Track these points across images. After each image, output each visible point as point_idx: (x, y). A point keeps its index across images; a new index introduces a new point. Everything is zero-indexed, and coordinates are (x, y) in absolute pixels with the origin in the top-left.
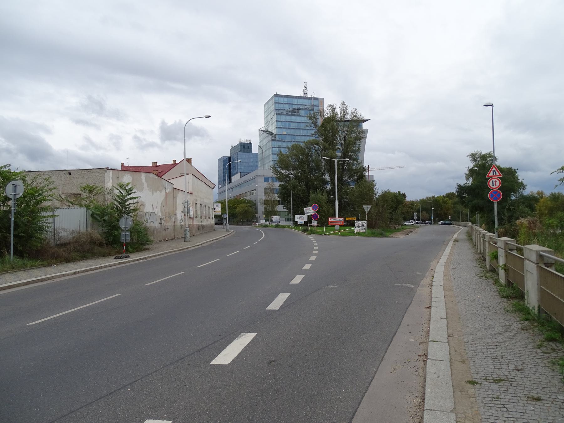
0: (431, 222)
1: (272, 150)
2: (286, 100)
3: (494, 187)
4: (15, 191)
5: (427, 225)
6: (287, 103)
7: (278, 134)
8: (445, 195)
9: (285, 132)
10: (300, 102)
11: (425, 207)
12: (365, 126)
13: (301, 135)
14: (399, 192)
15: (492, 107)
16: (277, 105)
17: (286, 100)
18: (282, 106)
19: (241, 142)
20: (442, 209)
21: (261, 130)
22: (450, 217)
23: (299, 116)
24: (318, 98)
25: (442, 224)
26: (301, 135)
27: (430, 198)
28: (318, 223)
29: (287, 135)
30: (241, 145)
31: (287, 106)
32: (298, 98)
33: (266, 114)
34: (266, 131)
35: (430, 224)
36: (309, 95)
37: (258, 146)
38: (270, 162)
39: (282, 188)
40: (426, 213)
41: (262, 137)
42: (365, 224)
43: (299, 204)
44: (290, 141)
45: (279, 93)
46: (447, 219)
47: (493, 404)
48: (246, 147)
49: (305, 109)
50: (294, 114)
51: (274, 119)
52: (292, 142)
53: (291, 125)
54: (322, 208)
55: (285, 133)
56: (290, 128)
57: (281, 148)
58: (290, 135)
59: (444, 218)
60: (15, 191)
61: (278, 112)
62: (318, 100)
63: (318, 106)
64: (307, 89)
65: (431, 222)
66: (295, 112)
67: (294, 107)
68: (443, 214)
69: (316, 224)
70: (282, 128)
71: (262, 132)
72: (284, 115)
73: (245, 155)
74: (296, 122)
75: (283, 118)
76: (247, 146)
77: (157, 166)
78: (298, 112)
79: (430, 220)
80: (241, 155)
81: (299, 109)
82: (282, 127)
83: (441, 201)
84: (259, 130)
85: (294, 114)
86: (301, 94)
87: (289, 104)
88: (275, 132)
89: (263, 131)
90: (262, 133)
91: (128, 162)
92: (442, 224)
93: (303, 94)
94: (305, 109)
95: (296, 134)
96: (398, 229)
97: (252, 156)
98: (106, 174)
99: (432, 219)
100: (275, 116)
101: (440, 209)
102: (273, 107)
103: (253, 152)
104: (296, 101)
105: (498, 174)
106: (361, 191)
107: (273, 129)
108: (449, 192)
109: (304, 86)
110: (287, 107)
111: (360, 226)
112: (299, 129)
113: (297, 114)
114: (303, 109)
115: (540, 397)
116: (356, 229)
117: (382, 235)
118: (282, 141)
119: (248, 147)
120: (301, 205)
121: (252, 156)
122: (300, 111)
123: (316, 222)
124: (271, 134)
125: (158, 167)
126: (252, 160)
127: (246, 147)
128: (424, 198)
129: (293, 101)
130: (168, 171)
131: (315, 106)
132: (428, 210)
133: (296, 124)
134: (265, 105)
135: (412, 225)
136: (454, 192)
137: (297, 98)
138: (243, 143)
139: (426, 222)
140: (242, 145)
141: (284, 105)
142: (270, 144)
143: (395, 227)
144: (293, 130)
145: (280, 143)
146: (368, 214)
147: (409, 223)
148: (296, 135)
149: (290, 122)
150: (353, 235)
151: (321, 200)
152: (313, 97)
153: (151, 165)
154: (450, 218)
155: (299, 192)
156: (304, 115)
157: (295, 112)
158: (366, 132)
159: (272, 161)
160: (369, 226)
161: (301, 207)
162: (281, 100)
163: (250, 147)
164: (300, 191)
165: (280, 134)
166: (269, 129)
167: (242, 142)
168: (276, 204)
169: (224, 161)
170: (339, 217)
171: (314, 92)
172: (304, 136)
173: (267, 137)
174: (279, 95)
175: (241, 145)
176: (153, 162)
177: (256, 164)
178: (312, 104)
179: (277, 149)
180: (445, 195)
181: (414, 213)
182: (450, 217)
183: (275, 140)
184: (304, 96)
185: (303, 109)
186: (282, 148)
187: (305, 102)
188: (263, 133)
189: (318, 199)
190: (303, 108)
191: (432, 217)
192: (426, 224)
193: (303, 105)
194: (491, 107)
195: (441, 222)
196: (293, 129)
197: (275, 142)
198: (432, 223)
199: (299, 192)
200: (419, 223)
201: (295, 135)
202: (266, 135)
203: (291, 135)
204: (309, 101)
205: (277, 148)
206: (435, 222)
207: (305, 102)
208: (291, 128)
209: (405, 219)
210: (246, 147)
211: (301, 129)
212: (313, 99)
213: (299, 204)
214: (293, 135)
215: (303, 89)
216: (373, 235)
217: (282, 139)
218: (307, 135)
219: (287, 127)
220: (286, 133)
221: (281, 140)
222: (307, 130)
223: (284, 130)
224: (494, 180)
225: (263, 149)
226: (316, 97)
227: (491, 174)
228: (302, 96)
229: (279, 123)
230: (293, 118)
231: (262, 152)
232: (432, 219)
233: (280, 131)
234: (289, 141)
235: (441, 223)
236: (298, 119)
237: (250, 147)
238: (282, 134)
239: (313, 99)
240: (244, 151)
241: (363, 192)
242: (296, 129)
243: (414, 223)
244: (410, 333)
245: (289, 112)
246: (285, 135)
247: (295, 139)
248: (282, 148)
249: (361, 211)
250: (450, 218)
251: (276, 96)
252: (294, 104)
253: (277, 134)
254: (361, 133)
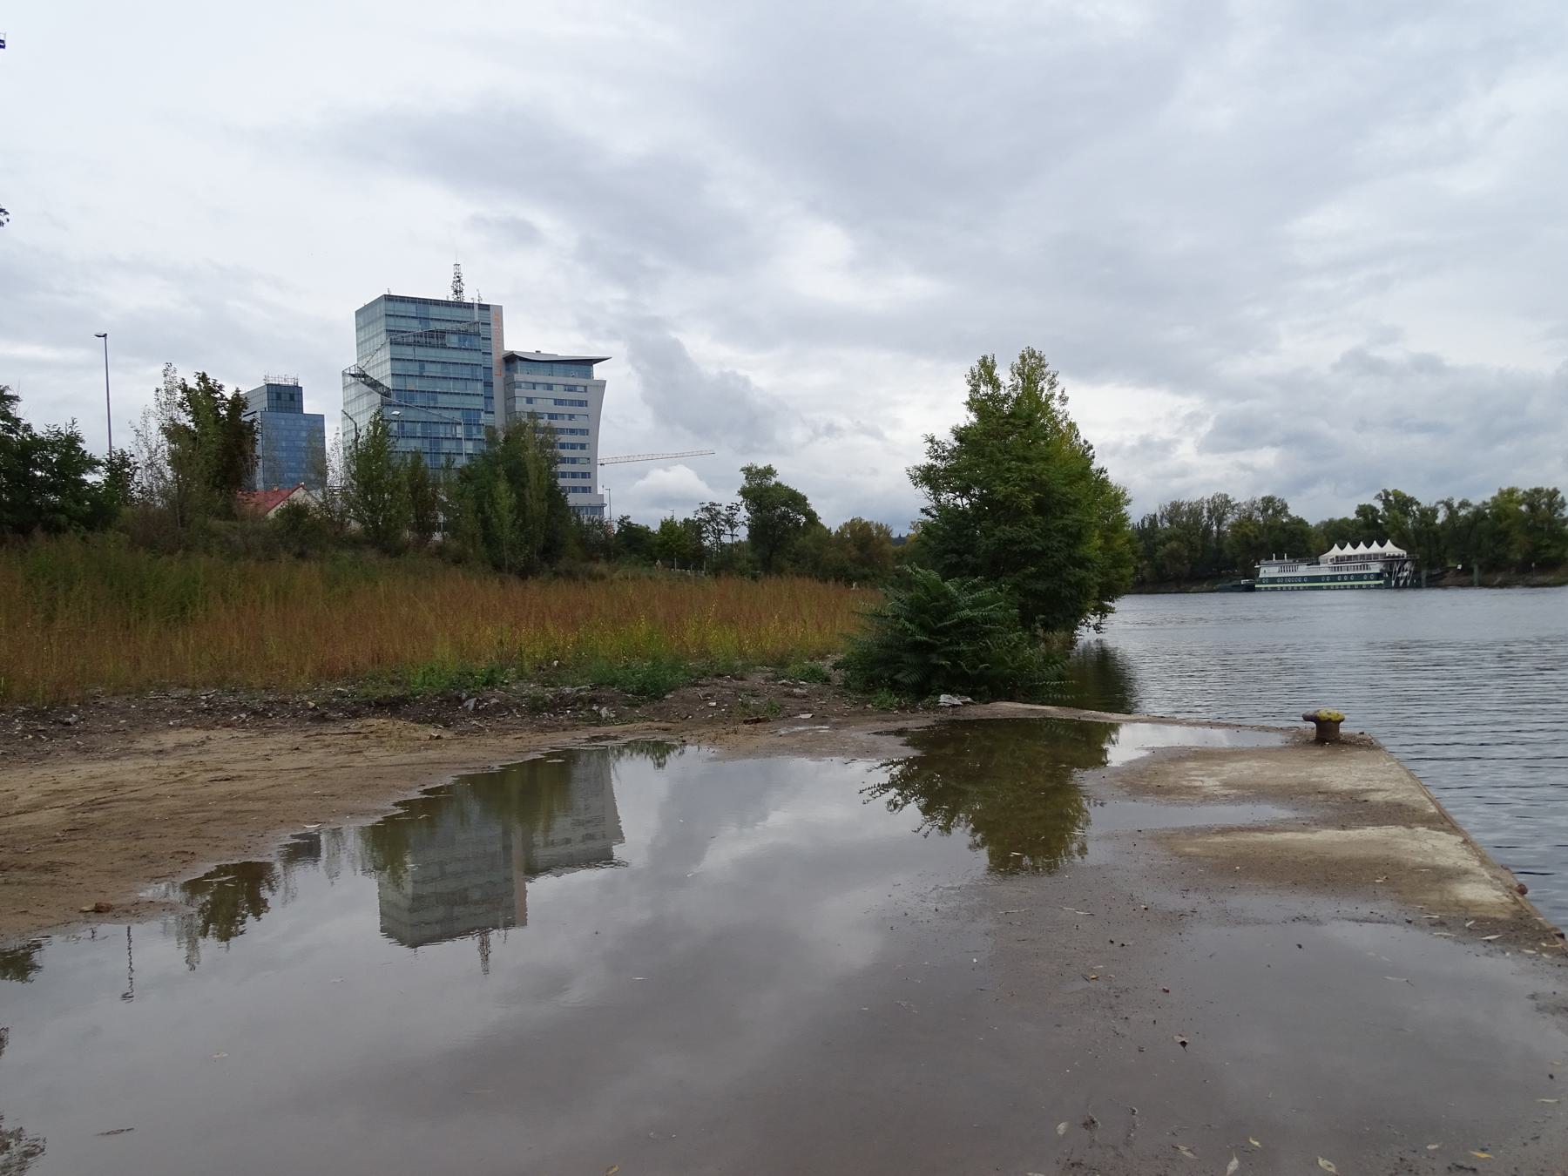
2: (412, 309)
12: (598, 371)
16: (391, 320)
17: (412, 309)
18: (403, 324)
19: (270, 382)
21: (348, 372)
23: (444, 347)
24: (488, 306)
26: (451, 393)
31: (415, 323)
36: (467, 298)
45: (396, 292)
47: (1488, 765)
61: (396, 339)
62: (489, 310)
66: (435, 338)
67: (434, 326)
71: (353, 380)
72: (409, 344)
73: (283, 420)
74: (439, 362)
75: (408, 352)
84: (344, 374)
86: (446, 294)
88: (388, 383)
95: (438, 390)
97: (303, 423)
100: (388, 347)
103: (305, 412)
104: (434, 312)
107: (382, 372)
110: (416, 326)
112: (446, 378)
115: (1454, 863)
119: (292, 398)
121: (303, 423)
124: (374, 385)
127: (285, 397)
138: (275, 385)
140: (274, 391)
148: (440, 393)
152: (476, 302)
156: (456, 346)
158: (601, 385)
162: (401, 308)
163: (296, 399)
167: (274, 383)
171: (478, 290)
174: (396, 296)
185: (453, 333)
187: (458, 313)
201: (436, 392)
204: (466, 312)
207: (458, 313)
210: (285, 397)
211: (451, 378)
212: (476, 307)
215: (451, 279)
220: (416, 387)
225: (357, 422)
226: (482, 303)
230: (432, 354)
231: (353, 427)
239: (476, 307)
244: (1168, 991)
247: (436, 402)
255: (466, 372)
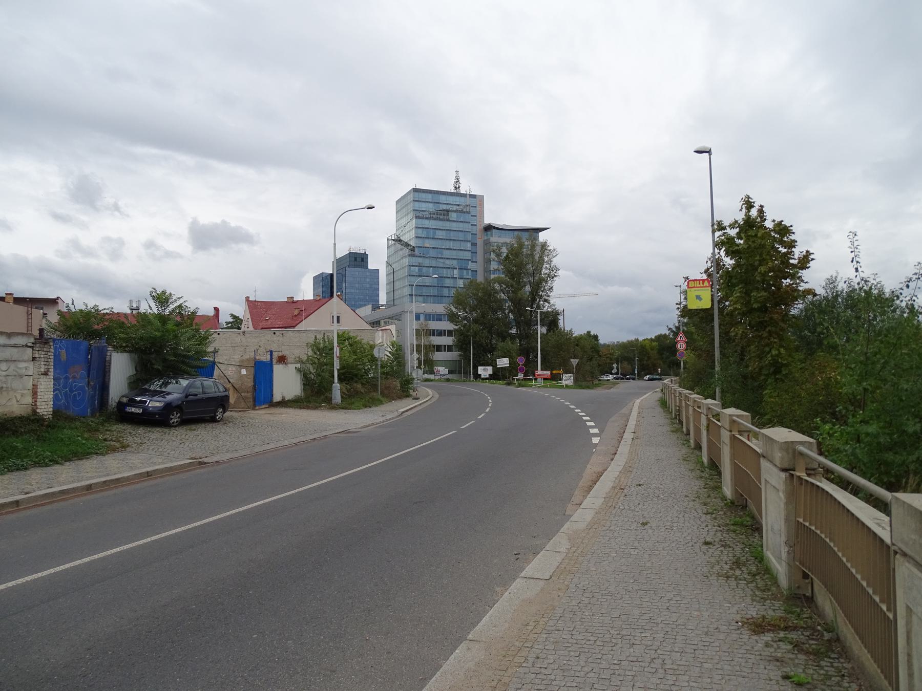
0: (634, 377)
1: (410, 269)
2: (429, 197)
3: (681, 348)
4: (379, 353)
5: (629, 380)
6: (431, 201)
7: (419, 247)
8: (653, 338)
9: (428, 243)
10: (450, 199)
11: (626, 355)
13: (452, 248)
14: (589, 332)
15: (710, 155)
17: (429, 197)
18: (423, 206)
20: (649, 358)
22: (659, 370)
23: (448, 220)
24: (475, 195)
25: (649, 379)
26: (451, 249)
27: (632, 341)
28: (524, 376)
29: (431, 248)
30: (351, 256)
32: (447, 195)
33: (399, 215)
34: (398, 240)
35: (634, 379)
37: (385, 263)
38: (405, 287)
39: (460, 333)
40: (628, 364)
41: (392, 249)
42: (572, 377)
43: (481, 353)
44: (435, 258)
46: (656, 373)
48: (358, 260)
49: (457, 211)
50: (441, 217)
51: (413, 223)
52: (438, 258)
53: (437, 234)
54: (513, 359)
55: (428, 246)
56: (435, 238)
57: (421, 266)
58: (435, 248)
59: (652, 371)
60: (379, 353)
61: (419, 215)
62: (476, 198)
63: (476, 207)
64: (460, 181)
65: (634, 377)
68: (651, 365)
69: (522, 377)
70: (424, 238)
71: (393, 242)
72: (426, 218)
74: (444, 230)
75: (427, 223)
76: (360, 259)
77: (293, 302)
78: (447, 215)
79: (633, 374)
80: (349, 271)
81: (448, 211)
82: (423, 236)
83: (648, 347)
85: (441, 217)
86: (450, 188)
87: (434, 203)
88: (412, 243)
89: (394, 240)
90: (391, 243)
91: (255, 296)
92: (649, 379)
93: (454, 188)
94: (457, 211)
95: (444, 247)
96: (596, 384)
97: (368, 274)
98: (376, 334)
99: (636, 372)
100: (414, 221)
101: (646, 358)
102: (410, 207)
104: (443, 199)
105: (684, 339)
106: (558, 341)
107: (409, 237)
108: (660, 334)
109: (456, 177)
110: (431, 207)
111: (568, 379)
113: (445, 218)
114: (454, 211)
116: (564, 383)
117: (588, 387)
118: (424, 257)
119: (362, 260)
120: (483, 355)
121: (368, 274)
122: (450, 213)
123: (523, 375)
124: (407, 245)
125: (295, 304)
126: (368, 280)
128: (625, 341)
129: (441, 199)
130: (317, 310)
131: (472, 206)
132: (630, 360)
133: (444, 232)
134: (396, 202)
135: (609, 380)
136: (667, 334)
137: (445, 195)
139: (628, 376)
141: (427, 204)
142: (406, 261)
143: (593, 382)
144: (440, 241)
145: (420, 260)
146: (576, 367)
147: (605, 378)
148: (444, 249)
149: (435, 229)
150: (562, 387)
151: (510, 349)
153: (286, 300)
154: (659, 372)
155: (481, 339)
157: (444, 215)
159: (410, 285)
160: (576, 380)
161: (483, 357)
164: (482, 338)
165: (421, 247)
166: (404, 238)
167: (353, 252)
168: (433, 351)
169: (323, 280)
170: (542, 370)
172: (455, 250)
173: (401, 250)
175: (351, 256)
176: (289, 296)
177: (374, 286)
178: (467, 204)
179: (417, 268)
180: (653, 338)
181: (614, 365)
182: (659, 370)
183: (414, 256)
184: (455, 191)
185: (454, 211)
186: (424, 266)
187: (457, 200)
188: (394, 244)
189: (508, 349)
190: (455, 209)
191: (636, 370)
192: (628, 379)
193: (455, 205)
194: (708, 154)
195: (648, 376)
196: (440, 239)
197: (414, 258)
198: (636, 379)
199: (481, 339)
200: (617, 379)
201: (442, 249)
202: (398, 246)
203: (437, 248)
204: (463, 199)
205: (417, 266)
206: (640, 377)
207: (457, 200)
208: (438, 239)
209: (603, 373)
211: (451, 240)
212: (468, 196)
213: (481, 353)
214: (440, 248)
216: (581, 387)
217: (423, 254)
218: (461, 249)
219: (432, 237)
220: (430, 245)
221: (421, 255)
222: (460, 242)
223: (427, 241)
224: (681, 343)
227: (679, 339)
228: (452, 191)
229: (420, 231)
232: (636, 372)
233: (420, 243)
234: (433, 257)
235: (647, 379)
236: (447, 225)
237: (364, 259)
238: (423, 247)
239: (468, 196)
240: (355, 266)
241: (560, 341)
242: (444, 239)
243: (611, 377)
245: (434, 214)
246: (428, 247)
247: (442, 255)
248: (424, 266)
249: (558, 363)
250: (659, 372)
251: (416, 190)
252: (441, 203)
253: (417, 247)
254: (555, 271)
255: (461, 236)
